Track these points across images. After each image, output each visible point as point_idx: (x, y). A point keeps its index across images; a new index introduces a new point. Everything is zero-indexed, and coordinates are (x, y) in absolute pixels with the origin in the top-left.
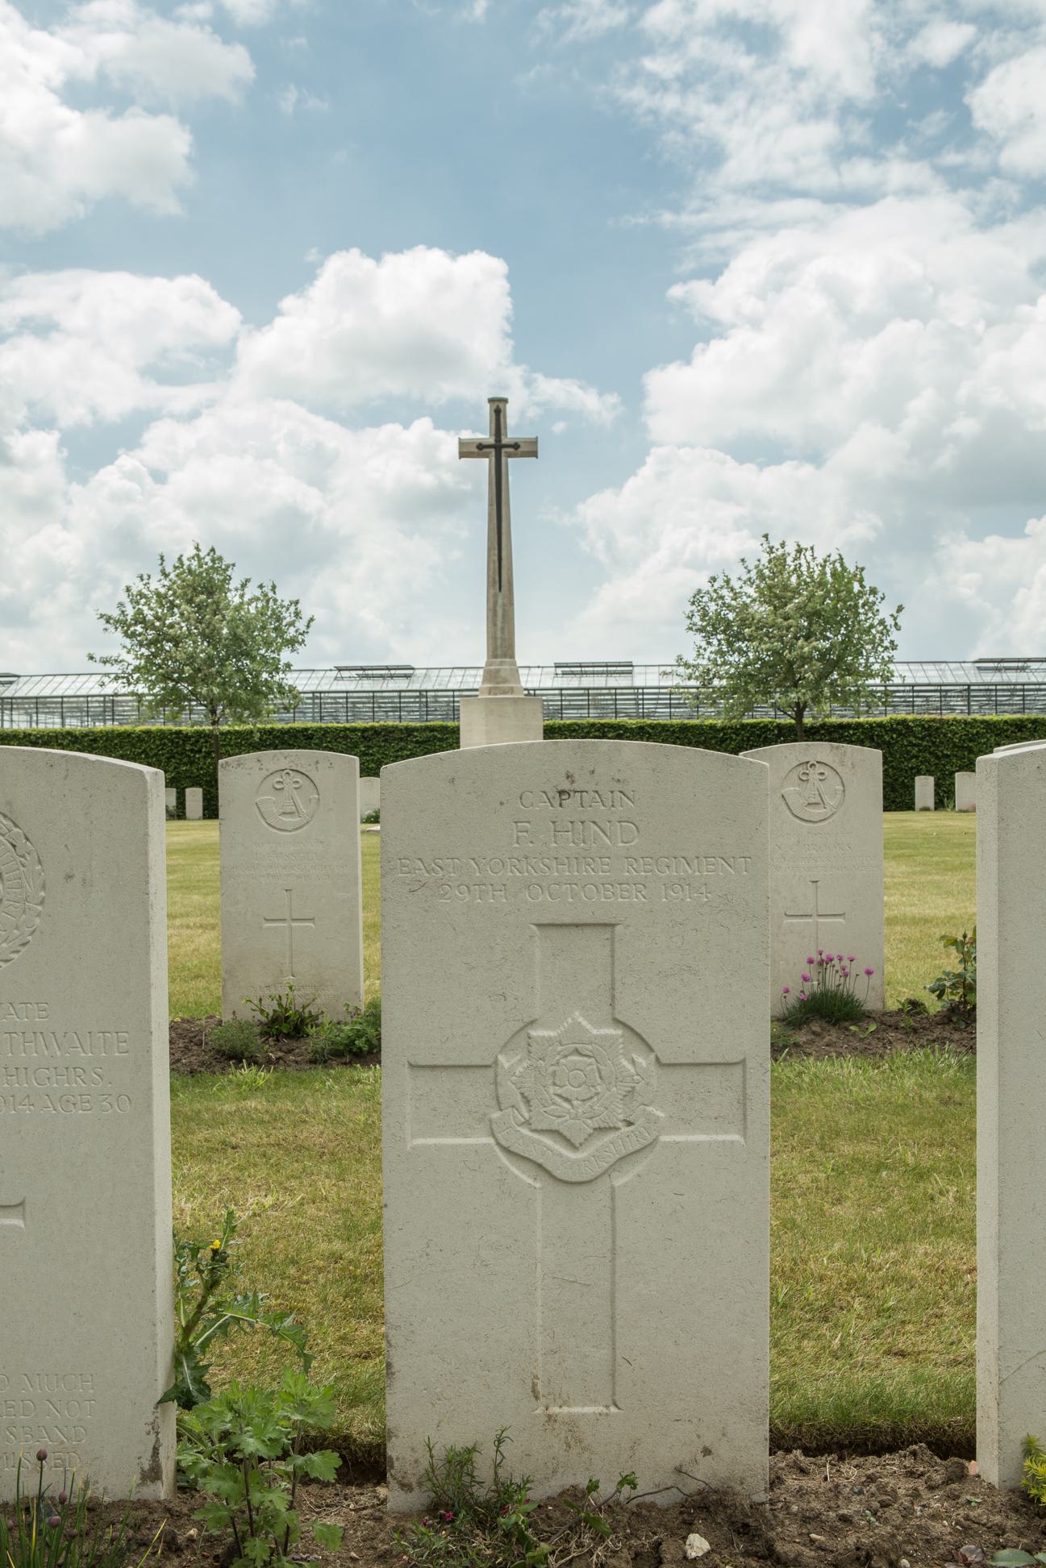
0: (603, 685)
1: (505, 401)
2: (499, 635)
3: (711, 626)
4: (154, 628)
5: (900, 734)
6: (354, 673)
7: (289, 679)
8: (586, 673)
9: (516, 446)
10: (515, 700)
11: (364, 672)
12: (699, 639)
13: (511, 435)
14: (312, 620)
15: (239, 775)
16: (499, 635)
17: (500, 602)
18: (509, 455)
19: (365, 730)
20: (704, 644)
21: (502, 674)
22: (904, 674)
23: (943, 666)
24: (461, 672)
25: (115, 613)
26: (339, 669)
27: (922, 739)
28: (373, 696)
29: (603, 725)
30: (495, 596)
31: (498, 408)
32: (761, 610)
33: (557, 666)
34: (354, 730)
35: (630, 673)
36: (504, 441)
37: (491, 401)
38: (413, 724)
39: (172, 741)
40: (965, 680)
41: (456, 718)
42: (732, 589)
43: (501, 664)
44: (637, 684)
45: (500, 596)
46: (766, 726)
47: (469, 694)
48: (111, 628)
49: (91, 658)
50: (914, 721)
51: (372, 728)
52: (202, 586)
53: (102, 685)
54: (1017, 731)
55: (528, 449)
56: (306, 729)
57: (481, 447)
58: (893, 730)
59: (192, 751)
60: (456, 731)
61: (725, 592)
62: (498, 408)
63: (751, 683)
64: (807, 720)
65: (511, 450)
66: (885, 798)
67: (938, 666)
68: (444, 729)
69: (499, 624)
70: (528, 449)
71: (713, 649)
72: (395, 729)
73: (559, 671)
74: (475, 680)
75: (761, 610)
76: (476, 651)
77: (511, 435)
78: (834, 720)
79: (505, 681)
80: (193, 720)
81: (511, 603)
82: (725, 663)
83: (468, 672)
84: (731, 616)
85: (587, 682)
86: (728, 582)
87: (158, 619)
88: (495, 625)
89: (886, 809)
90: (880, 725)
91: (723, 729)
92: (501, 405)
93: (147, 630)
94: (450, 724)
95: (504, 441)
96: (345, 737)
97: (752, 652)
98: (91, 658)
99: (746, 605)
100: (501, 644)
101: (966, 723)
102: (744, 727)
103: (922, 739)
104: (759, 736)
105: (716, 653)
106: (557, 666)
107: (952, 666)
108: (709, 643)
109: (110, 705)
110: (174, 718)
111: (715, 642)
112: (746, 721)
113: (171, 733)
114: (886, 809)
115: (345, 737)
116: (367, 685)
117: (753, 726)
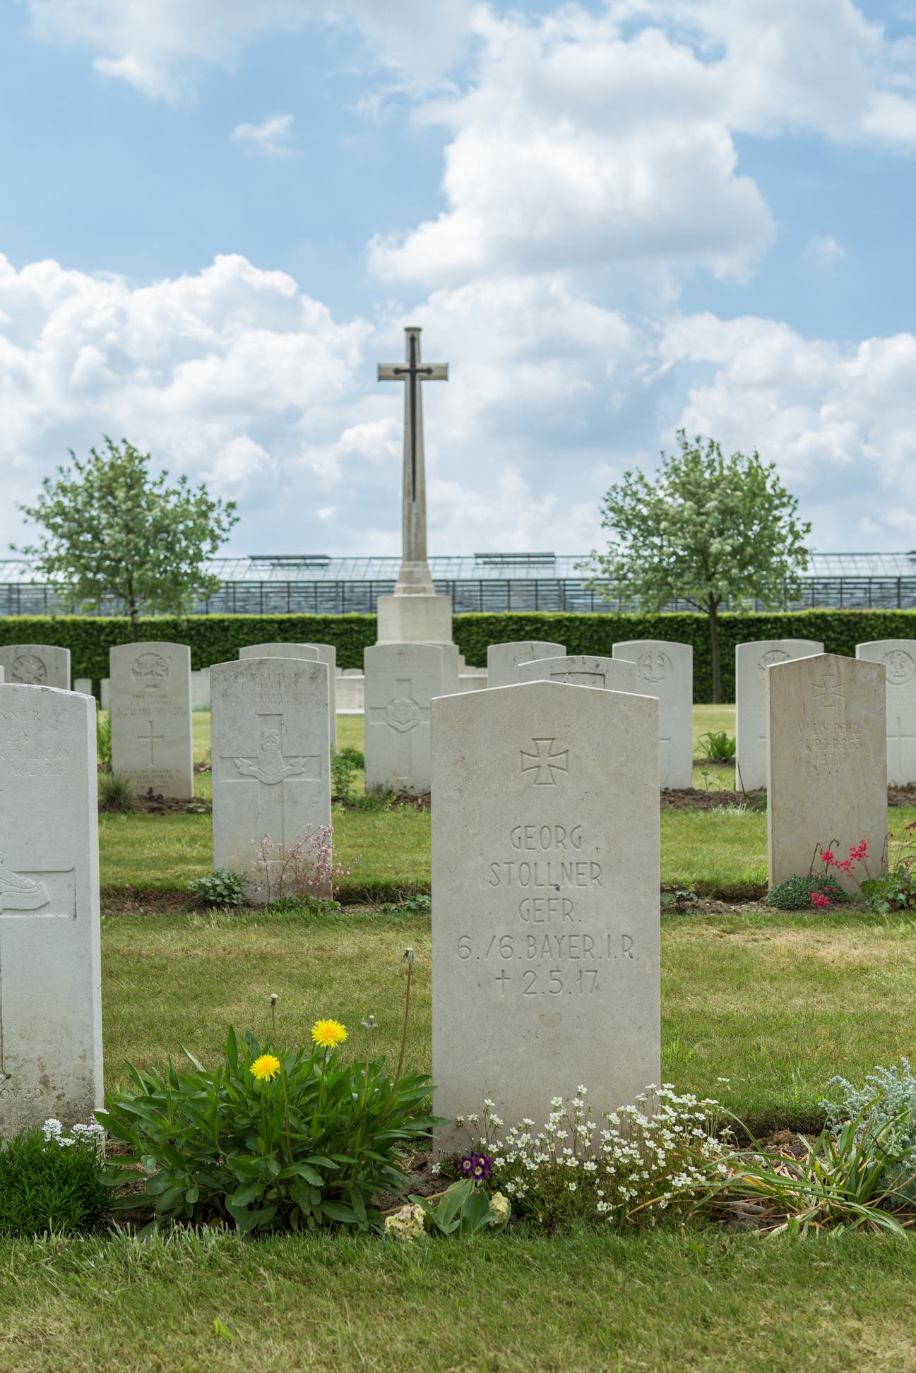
0: (524, 577)
1: (419, 330)
2: (413, 540)
3: (624, 520)
4: (74, 520)
5: (818, 628)
6: (267, 562)
7: (205, 568)
8: (508, 563)
9: (429, 371)
10: (427, 599)
11: (278, 561)
12: (613, 535)
13: (425, 361)
14: (238, 520)
15: (120, 656)
16: (413, 540)
17: (414, 511)
18: (423, 379)
19: (281, 622)
20: (618, 539)
21: (415, 575)
22: (817, 568)
23: (875, 558)
24: (379, 562)
25: (36, 505)
26: (253, 558)
27: (841, 633)
28: (288, 587)
29: (521, 619)
30: (410, 505)
31: (413, 336)
32: (675, 503)
33: (477, 556)
34: (271, 622)
35: (552, 563)
36: (419, 366)
37: (407, 330)
38: (330, 616)
39: (87, 632)
40: (897, 574)
41: (373, 608)
42: (646, 486)
43: (415, 566)
44: (558, 576)
45: (414, 505)
46: (683, 620)
47: (387, 587)
48: (32, 519)
49: (12, 548)
50: (832, 615)
51: (289, 620)
52: (122, 479)
53: (23, 572)
54: (888, 628)
55: (439, 373)
56: (222, 621)
57: (397, 371)
58: (811, 624)
59: (105, 641)
60: (373, 624)
61: (639, 487)
62: (413, 336)
63: (660, 581)
64: (724, 614)
65: (424, 374)
66: (695, 690)
67: (869, 558)
68: (360, 621)
69: (413, 531)
70: (439, 373)
71: (628, 544)
72: (312, 621)
73: (480, 561)
74: (392, 571)
75: (675, 503)
76: (391, 543)
77: (425, 361)
78: (752, 614)
79: (418, 581)
80: (112, 613)
81: (424, 512)
82: (639, 557)
83: (385, 562)
84: (645, 512)
85: (509, 573)
86: (641, 478)
87: (78, 511)
88: (409, 531)
89: (695, 702)
90: (799, 619)
91: (640, 622)
92: (415, 334)
93: (70, 522)
94: (368, 616)
95: (419, 366)
96: (262, 629)
97: (674, 547)
98: (12, 548)
99: (660, 501)
100: (415, 550)
101: (885, 617)
102: (661, 620)
103: (841, 633)
104: (677, 630)
105: (632, 547)
106: (477, 556)
107: (884, 557)
108: (624, 538)
109: (43, 598)
110: (90, 610)
111: (630, 537)
112: (663, 614)
113: (85, 623)
114: (695, 702)
115: (262, 629)
116: (282, 575)
117: (671, 620)
